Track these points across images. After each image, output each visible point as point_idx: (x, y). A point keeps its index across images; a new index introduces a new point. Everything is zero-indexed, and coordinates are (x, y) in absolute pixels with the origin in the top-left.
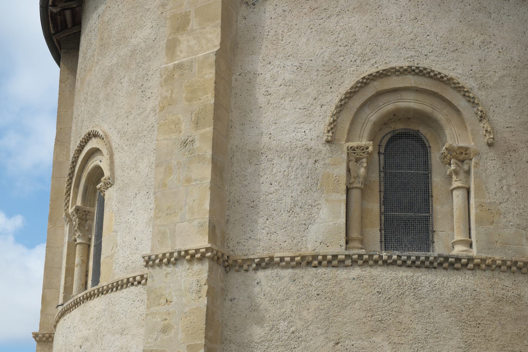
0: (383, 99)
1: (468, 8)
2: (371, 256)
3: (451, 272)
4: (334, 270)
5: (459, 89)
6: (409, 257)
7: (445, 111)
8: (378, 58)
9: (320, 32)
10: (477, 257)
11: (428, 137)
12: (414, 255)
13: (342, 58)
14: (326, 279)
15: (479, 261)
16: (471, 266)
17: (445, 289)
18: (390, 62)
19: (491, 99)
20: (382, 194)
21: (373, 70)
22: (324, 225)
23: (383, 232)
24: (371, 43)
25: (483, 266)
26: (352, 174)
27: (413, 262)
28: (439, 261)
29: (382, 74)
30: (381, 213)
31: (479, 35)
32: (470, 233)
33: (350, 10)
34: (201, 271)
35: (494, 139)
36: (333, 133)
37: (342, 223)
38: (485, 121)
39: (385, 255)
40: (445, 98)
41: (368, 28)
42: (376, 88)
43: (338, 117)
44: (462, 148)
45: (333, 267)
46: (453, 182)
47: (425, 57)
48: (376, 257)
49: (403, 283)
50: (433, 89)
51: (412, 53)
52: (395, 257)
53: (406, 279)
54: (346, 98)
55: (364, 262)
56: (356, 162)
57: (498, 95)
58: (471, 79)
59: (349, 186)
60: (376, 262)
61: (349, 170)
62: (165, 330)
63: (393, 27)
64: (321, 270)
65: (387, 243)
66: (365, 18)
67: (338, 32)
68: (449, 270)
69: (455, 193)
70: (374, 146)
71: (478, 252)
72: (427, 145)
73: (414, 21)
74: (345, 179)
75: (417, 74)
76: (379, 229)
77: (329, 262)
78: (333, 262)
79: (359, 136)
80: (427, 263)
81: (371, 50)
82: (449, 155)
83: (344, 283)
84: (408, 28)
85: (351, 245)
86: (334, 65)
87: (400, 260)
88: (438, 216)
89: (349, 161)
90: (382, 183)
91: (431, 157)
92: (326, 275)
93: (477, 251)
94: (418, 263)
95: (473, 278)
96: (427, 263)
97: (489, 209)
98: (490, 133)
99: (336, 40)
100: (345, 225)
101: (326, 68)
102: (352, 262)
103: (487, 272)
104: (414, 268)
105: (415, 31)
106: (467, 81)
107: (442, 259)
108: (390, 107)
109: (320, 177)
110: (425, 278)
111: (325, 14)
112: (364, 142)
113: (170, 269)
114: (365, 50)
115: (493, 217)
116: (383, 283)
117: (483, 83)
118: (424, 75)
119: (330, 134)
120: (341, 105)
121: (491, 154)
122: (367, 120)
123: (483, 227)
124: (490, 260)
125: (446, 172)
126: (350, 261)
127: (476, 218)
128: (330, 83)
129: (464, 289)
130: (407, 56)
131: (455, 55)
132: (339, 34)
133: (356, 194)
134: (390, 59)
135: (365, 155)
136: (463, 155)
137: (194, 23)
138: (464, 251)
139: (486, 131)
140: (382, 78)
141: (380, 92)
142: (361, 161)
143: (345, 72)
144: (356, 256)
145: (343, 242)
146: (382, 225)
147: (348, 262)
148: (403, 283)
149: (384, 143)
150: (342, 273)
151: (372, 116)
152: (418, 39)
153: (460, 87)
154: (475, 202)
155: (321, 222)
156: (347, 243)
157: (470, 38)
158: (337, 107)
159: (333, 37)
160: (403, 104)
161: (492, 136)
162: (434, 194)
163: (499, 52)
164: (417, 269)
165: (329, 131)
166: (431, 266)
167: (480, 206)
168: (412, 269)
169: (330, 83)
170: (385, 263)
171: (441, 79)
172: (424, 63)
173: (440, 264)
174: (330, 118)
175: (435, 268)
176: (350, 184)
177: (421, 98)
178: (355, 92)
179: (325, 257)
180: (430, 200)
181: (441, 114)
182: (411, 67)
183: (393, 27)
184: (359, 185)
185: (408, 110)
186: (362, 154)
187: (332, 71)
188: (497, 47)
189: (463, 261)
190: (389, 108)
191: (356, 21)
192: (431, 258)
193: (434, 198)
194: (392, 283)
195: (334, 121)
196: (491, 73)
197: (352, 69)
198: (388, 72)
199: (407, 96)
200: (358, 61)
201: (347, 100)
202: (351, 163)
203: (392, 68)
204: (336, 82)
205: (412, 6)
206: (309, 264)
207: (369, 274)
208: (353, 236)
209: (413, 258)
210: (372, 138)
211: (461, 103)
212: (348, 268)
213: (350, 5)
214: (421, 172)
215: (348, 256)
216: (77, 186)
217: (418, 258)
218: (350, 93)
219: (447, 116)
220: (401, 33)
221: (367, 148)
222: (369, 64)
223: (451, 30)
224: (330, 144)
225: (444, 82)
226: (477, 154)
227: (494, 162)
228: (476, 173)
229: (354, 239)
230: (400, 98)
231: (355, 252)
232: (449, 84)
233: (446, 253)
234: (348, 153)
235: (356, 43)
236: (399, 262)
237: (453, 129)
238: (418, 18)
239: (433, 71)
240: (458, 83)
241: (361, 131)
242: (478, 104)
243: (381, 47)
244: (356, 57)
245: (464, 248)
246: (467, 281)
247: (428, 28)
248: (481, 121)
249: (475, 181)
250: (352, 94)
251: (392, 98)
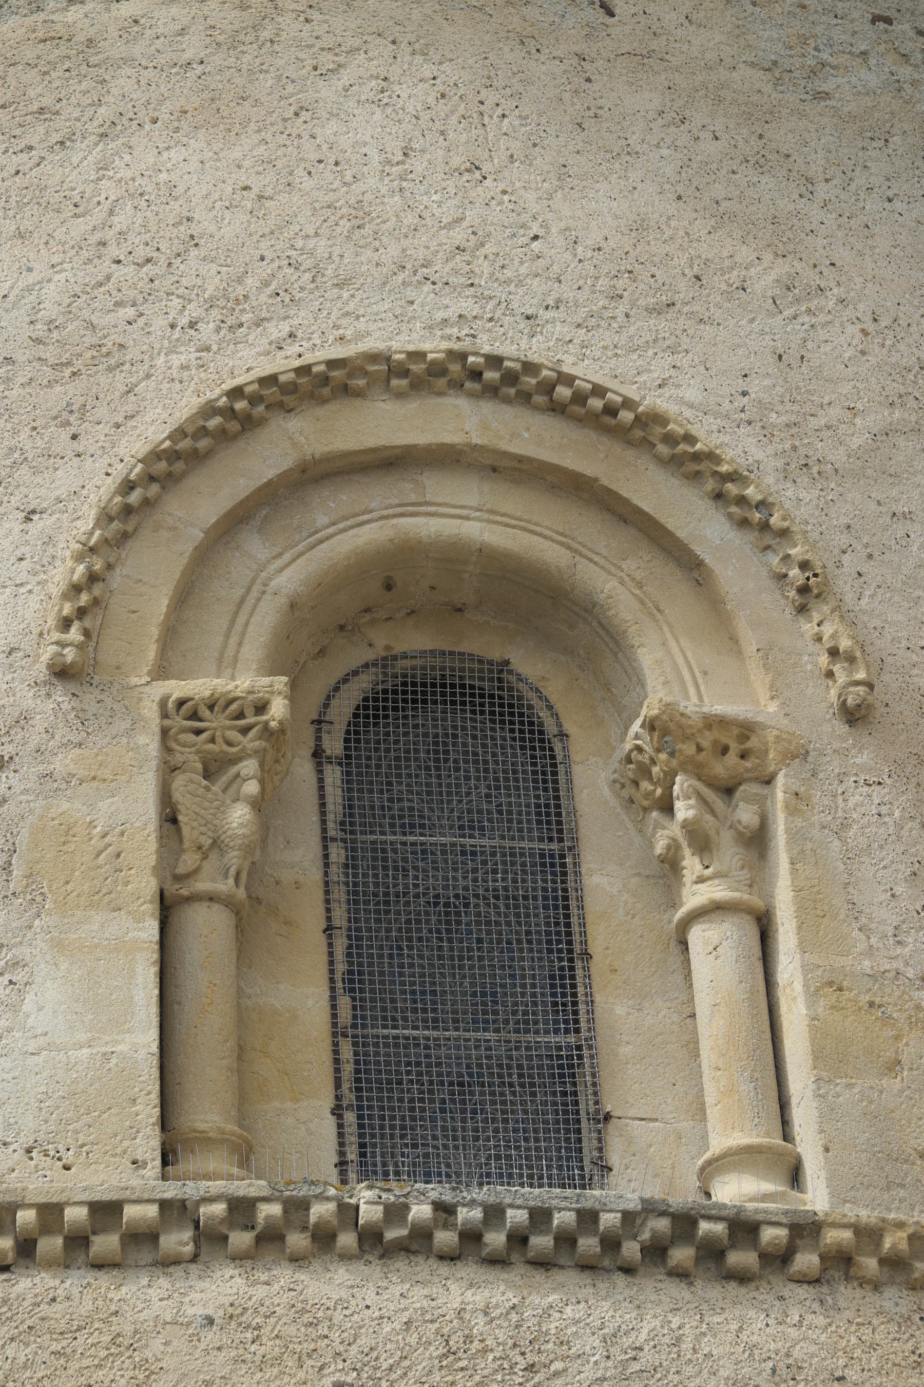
0: (326, 506)
1: (709, 147)
2: (297, 1207)
3: (712, 1291)
4: (103, 1280)
5: (691, 462)
6: (494, 1213)
7: (630, 565)
8: (301, 317)
9: (21, 206)
10: (836, 1217)
11: (554, 690)
12: (518, 1201)
13: (130, 312)
14: (62, 1326)
15: (847, 1235)
16: (806, 1260)
17: (689, 1370)
18: (360, 336)
19: (845, 520)
20: (341, 944)
21: (282, 364)
23: (350, 1117)
24: (269, 255)
25: (870, 1264)
26: (186, 830)
27: (519, 1239)
28: (646, 1236)
29: (324, 380)
30: (337, 1032)
31: (768, 256)
32: (785, 1122)
33: (164, 116)
35: (871, 686)
36: (87, 633)
37: (142, 1054)
38: (826, 609)
39: (368, 1202)
40: (627, 502)
41: (252, 195)
42: (295, 445)
43: (109, 567)
44: (722, 722)
45: (98, 1266)
46: (685, 891)
47: (523, 324)
48: (320, 1211)
49: (469, 1339)
50: (570, 461)
51: (468, 306)
52: (421, 1211)
53: (481, 1320)
54: (152, 479)
55: (259, 1239)
56: (208, 774)
57: (873, 506)
58: (744, 430)
59: (172, 889)
60: (324, 1238)
61: (170, 818)
63: (369, 197)
65: (365, 1156)
66: (237, 154)
67: (106, 206)
68: (699, 1283)
69: (697, 935)
70: (294, 691)
71: (834, 1194)
72: (550, 728)
73: (466, 176)
74: (152, 845)
75: (492, 391)
76: (328, 1102)
77: (78, 1242)
78: (99, 1238)
79: (220, 660)
80: (588, 1244)
81: (266, 284)
82: (663, 756)
83: (157, 1345)
84: (440, 204)
85: (188, 1164)
86: (90, 340)
87: (446, 1226)
88: (625, 1050)
89: (169, 770)
90: (339, 894)
91: (570, 781)
92: (57, 1307)
93: (832, 1195)
94: (541, 1242)
95: (821, 1321)
96: (588, 1244)
97: (871, 1004)
98: (851, 659)
99: (98, 236)
100: (155, 1061)
101: (50, 353)
102: (196, 1241)
103: (890, 1292)
104: (522, 1269)
105: (472, 215)
106: (726, 439)
107: (662, 1225)
108: (369, 535)
109: (23, 840)
110: (582, 1316)
111: (41, 129)
112: (244, 682)
114: (240, 280)
115: (897, 1038)
116: (364, 1341)
117: (802, 451)
118: (525, 398)
119: (74, 635)
120: (128, 510)
121: (864, 758)
122: (256, 588)
123: (850, 1086)
124: (902, 1235)
125: (651, 846)
126: (187, 1234)
127: (813, 1040)
128: (72, 417)
129: (782, 1371)
130: (440, 315)
131: (662, 324)
132: (111, 213)
133: (207, 929)
134: (361, 325)
135: (251, 742)
136: (732, 758)
138: (765, 1197)
139: (834, 652)
140: (324, 401)
141: (317, 461)
142: (233, 770)
143: (143, 369)
144: (219, 1208)
145: (148, 1145)
146: (345, 1086)
147: (178, 1240)
148: (469, 1339)
149: (342, 710)
150: (143, 1297)
151: (281, 572)
152: (489, 249)
153: (697, 457)
154: (806, 969)
155: (32, 1046)
156: (165, 1163)
157: (727, 263)
158: (105, 517)
159: (81, 226)
161: (861, 675)
162: (596, 947)
163: (864, 332)
164: (539, 1276)
165: (66, 624)
166: (606, 1263)
167: (828, 985)
168: (514, 1275)
169: (72, 417)
170: (372, 1242)
171: (608, 420)
173: (656, 1252)
174: (70, 563)
175: (628, 1270)
176: (178, 878)
177: (514, 501)
178: (196, 458)
179: (51, 1213)
180: (579, 972)
181: (612, 576)
182: (462, 356)
183: (369, 197)
184: (225, 886)
185: (452, 557)
186: (234, 735)
187: (78, 364)
188: (849, 313)
189: (768, 1234)
190: (361, 541)
191: (194, 165)
192: (609, 1220)
193: (598, 965)
194: (413, 1339)
195: (93, 578)
196: (835, 412)
197: (176, 360)
198: (350, 375)
199: (440, 487)
200: (207, 330)
201: (155, 488)
202: (179, 782)
203: (374, 357)
204: (101, 412)
205: (454, 119)
207: (287, 1297)
208: (202, 1126)
209: (516, 1216)
210: (286, 658)
211: (705, 528)
212: (177, 1271)
213: (163, 99)
214: (525, 844)
217: (540, 1217)
218: (172, 456)
219: (640, 585)
220: (410, 219)
221: (261, 708)
222: (259, 340)
223: (639, 227)
224: (72, 687)
225: (621, 433)
226: (798, 754)
227: (878, 794)
228: (794, 837)
229: (205, 1141)
230: (413, 498)
231: (211, 1184)
232: (647, 444)
233: (684, 1195)
234: (165, 732)
235: (194, 252)
236: (445, 1238)
237: (672, 643)
238: (486, 168)
239: (569, 380)
240: (689, 439)
241: (227, 636)
242: (784, 533)
243: (317, 273)
244: (194, 310)
245: (768, 1187)
246: (793, 1333)
247: (534, 207)
248: (802, 609)
249: (794, 872)
250: (179, 466)
251: (378, 494)
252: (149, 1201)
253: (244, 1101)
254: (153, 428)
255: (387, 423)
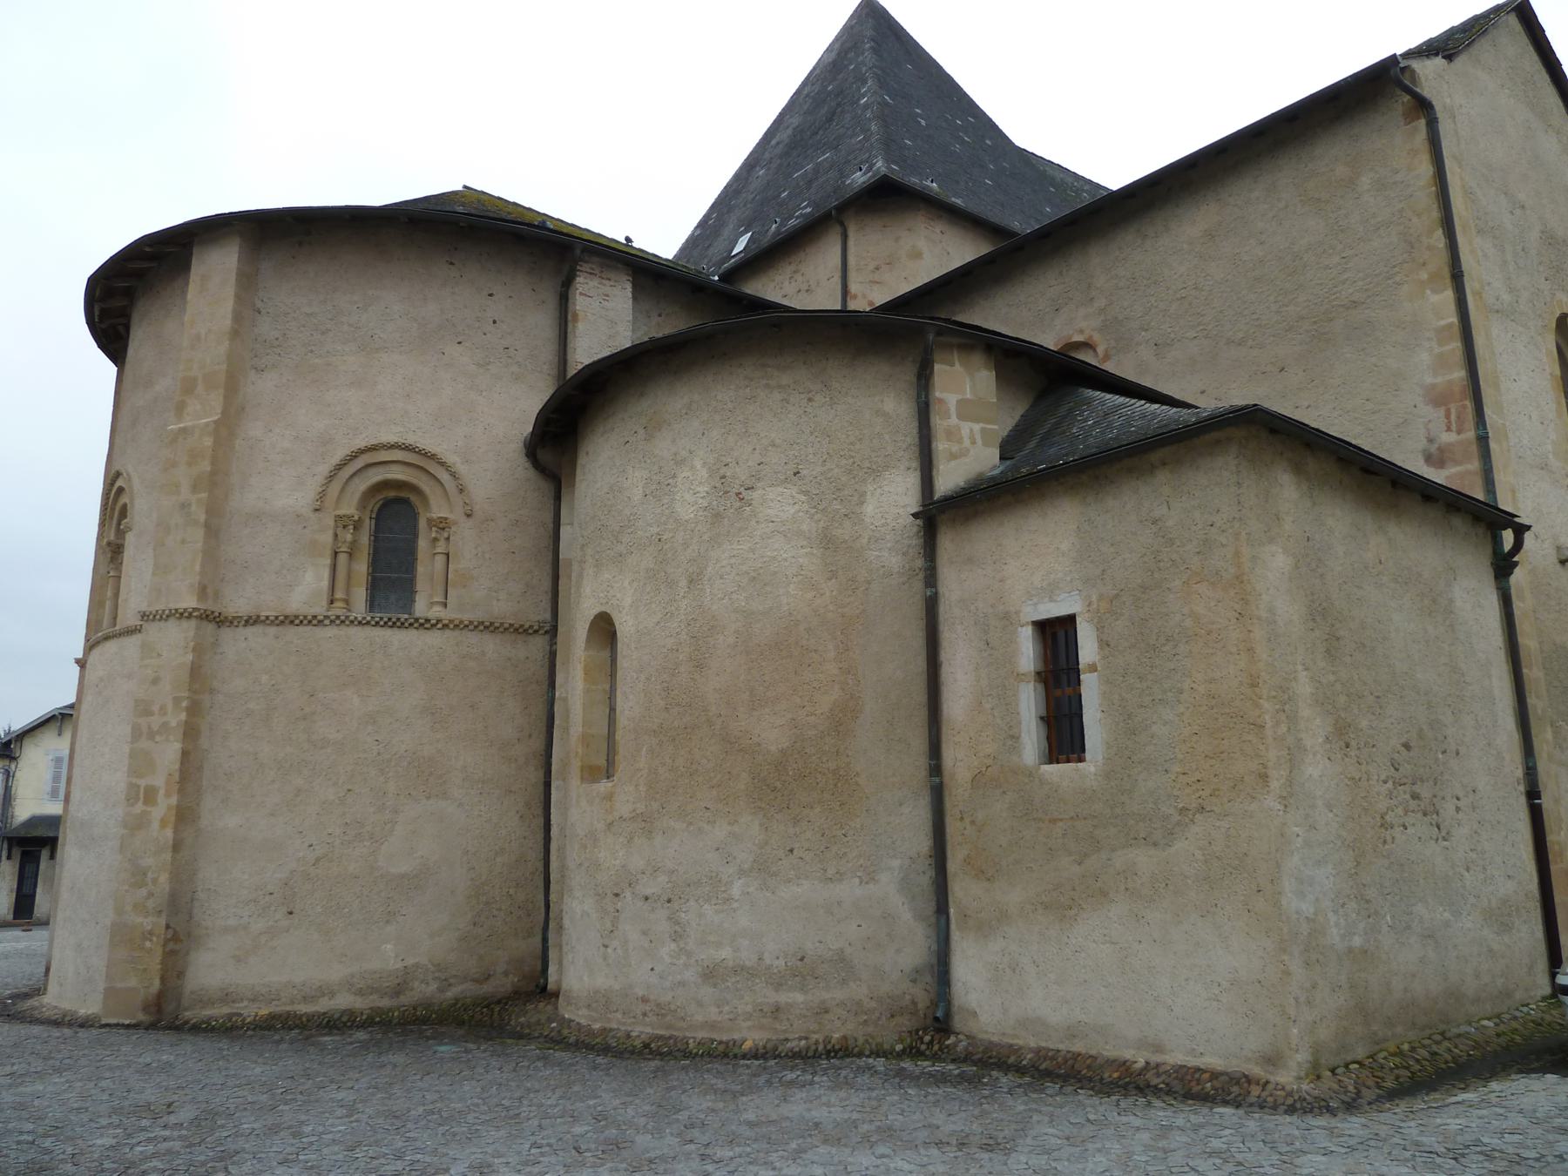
3: (422, 631)
22: (307, 587)
34: (238, 602)
61: (336, 535)
62: (155, 681)
64: (301, 628)
65: (372, 604)
78: (314, 621)
113: (162, 624)
137: (200, 388)
145: (325, 603)
151: (362, 484)
160: (390, 476)
172: (411, 439)
199: (394, 467)
206: (292, 622)
215: (326, 617)
216: (111, 518)
231: (338, 610)
251: (381, 469)
252: (662, 1054)
253: (348, 591)
254: (336, 460)
255: (384, 456)
